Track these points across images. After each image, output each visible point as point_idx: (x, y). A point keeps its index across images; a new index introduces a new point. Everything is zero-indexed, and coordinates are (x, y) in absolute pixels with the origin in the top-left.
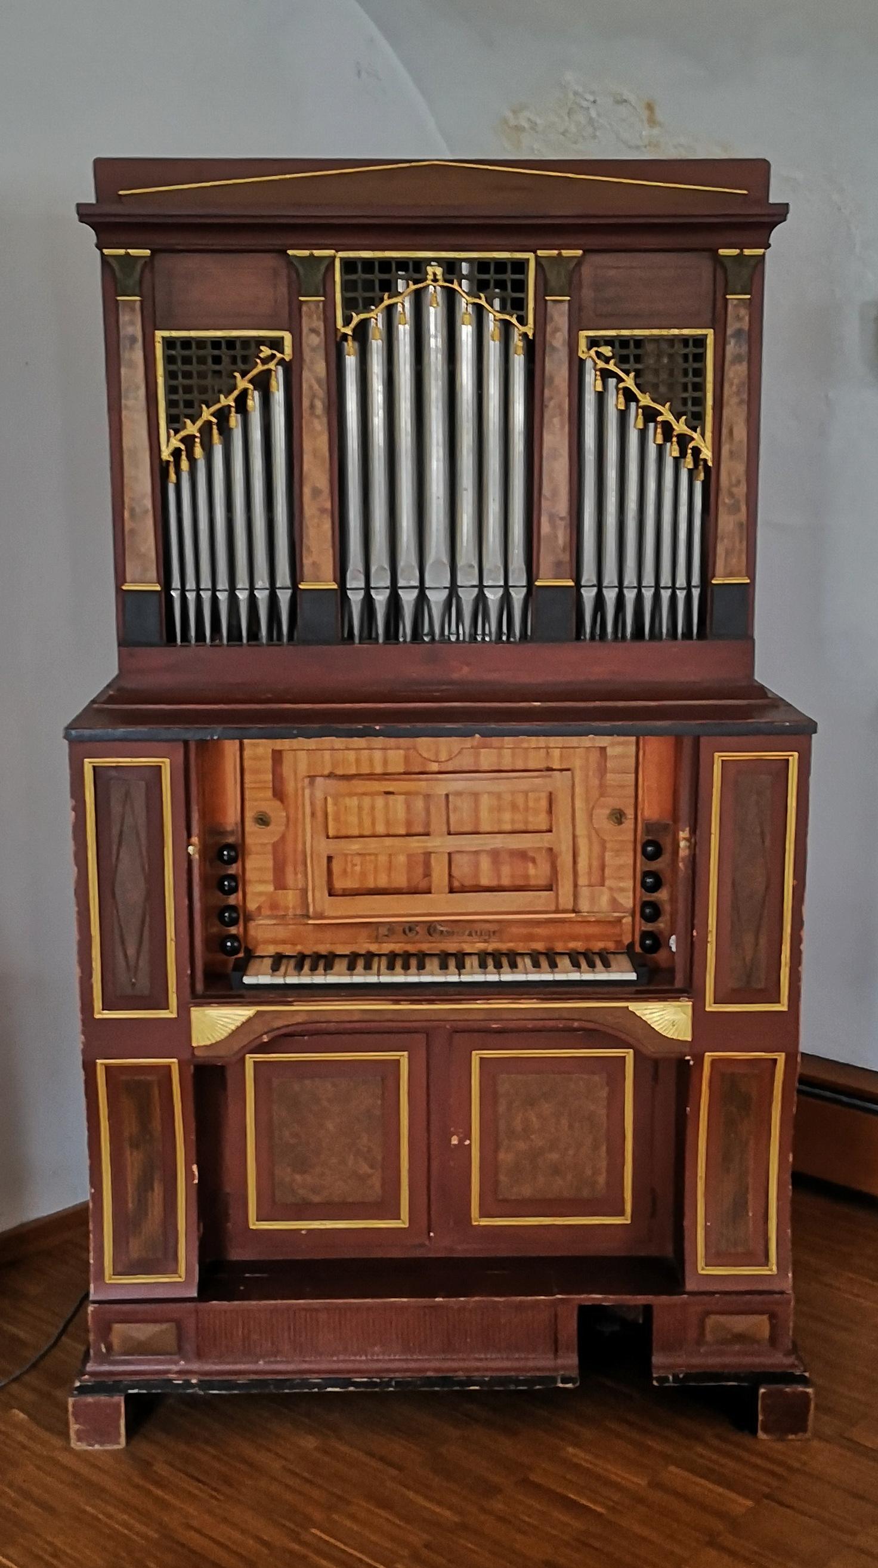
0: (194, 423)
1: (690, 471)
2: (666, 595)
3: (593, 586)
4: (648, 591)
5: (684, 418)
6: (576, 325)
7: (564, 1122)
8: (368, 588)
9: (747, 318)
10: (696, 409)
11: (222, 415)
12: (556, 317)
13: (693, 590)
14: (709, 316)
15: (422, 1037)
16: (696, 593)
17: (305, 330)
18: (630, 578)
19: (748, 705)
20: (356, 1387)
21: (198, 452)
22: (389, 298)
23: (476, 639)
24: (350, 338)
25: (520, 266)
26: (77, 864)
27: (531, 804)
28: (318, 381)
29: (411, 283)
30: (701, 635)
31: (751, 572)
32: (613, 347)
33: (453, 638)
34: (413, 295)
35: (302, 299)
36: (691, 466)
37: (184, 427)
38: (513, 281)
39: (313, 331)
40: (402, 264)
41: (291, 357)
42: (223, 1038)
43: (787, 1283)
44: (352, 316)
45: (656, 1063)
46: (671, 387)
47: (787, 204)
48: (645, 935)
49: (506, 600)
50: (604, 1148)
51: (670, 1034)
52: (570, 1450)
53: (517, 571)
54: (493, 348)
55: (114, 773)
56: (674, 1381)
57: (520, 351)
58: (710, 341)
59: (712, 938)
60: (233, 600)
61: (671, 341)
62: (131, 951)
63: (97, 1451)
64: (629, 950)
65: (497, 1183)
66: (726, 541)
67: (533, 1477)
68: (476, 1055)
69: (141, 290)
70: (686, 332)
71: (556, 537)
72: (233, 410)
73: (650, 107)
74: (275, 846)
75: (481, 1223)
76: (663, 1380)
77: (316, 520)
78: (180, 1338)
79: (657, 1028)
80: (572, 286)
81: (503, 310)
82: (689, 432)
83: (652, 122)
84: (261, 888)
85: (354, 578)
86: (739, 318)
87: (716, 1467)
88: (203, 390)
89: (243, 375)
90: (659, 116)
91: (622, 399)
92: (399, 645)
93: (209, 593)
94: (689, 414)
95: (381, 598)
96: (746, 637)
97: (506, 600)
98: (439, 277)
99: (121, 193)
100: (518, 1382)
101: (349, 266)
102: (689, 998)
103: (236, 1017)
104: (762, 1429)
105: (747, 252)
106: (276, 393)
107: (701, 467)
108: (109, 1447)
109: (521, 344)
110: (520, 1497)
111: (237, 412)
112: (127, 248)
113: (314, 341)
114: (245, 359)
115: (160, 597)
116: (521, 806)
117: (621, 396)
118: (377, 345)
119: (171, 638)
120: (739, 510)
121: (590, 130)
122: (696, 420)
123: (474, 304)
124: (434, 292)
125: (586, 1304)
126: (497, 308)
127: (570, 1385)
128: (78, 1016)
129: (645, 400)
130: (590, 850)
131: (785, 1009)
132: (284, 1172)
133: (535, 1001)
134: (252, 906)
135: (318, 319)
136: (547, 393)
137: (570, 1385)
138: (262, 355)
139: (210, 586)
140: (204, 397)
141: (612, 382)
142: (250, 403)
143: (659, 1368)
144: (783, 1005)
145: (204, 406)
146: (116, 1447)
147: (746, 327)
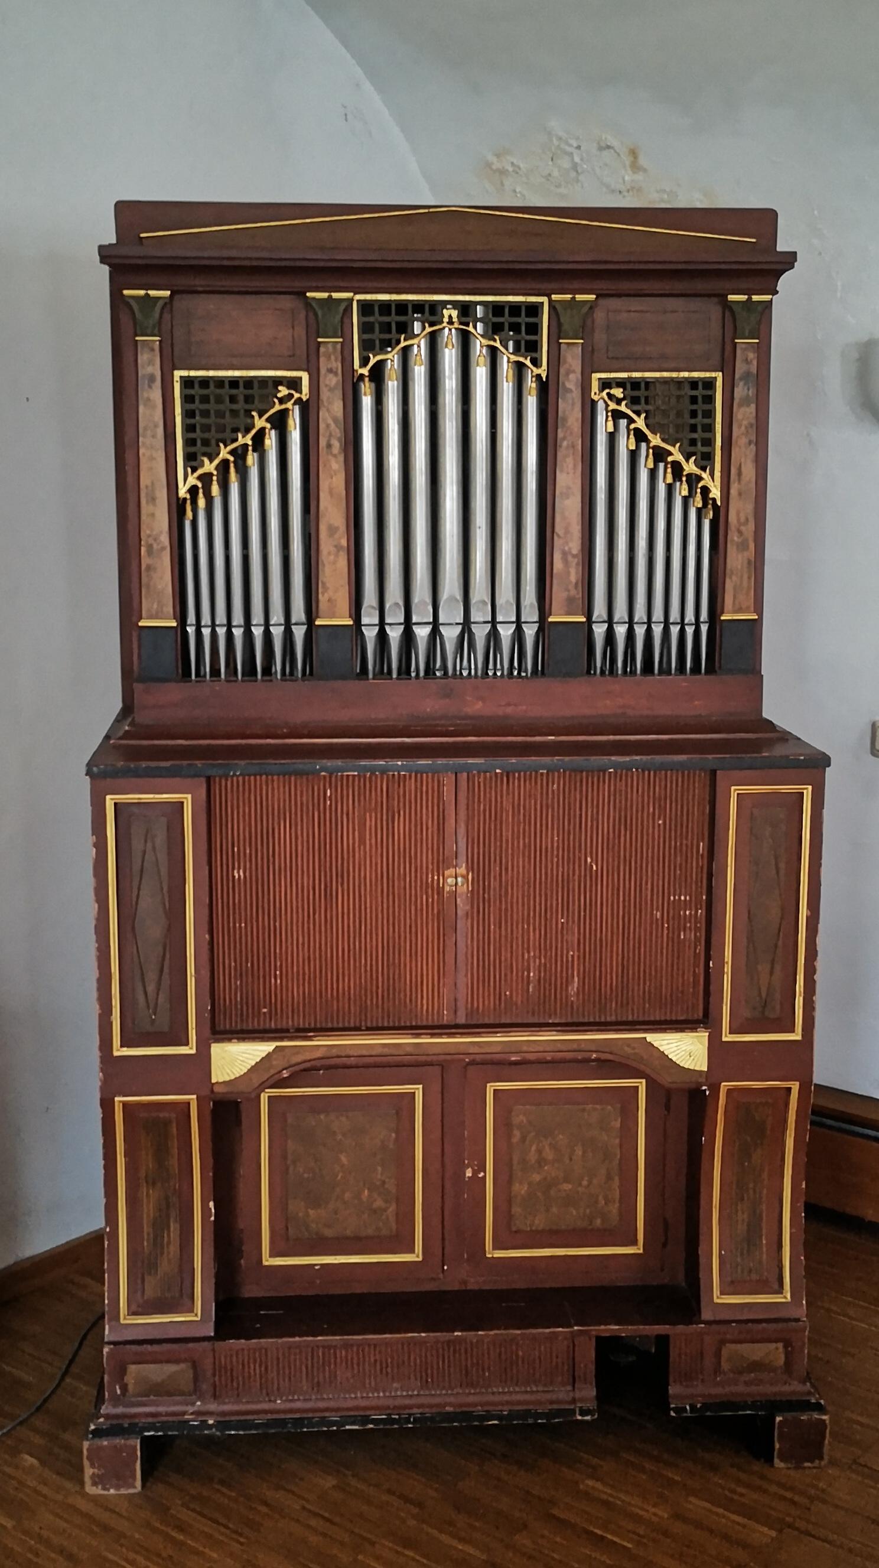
0: (211, 461)
1: (699, 511)
2: (675, 630)
3: (604, 622)
4: (600, 627)
5: (694, 458)
6: (589, 367)
7: (579, 1152)
8: (382, 623)
9: (755, 362)
10: (706, 449)
12: (569, 359)
13: (702, 626)
15: (437, 1070)
16: (704, 628)
17: (323, 371)
18: (640, 613)
19: (757, 739)
20: (384, 1425)
21: (215, 489)
22: (405, 340)
23: (487, 674)
24: (367, 379)
25: (534, 310)
26: (97, 901)
28: (335, 420)
29: (427, 325)
30: (711, 670)
31: (759, 608)
32: (625, 389)
33: (465, 673)
34: (428, 336)
35: (320, 340)
36: (700, 505)
37: (202, 465)
39: (330, 371)
40: (419, 307)
41: (308, 397)
42: (242, 1073)
43: (801, 1312)
45: (669, 1093)
46: (678, 428)
47: (795, 253)
49: (519, 635)
51: (687, 1064)
52: (590, 1482)
53: (528, 608)
54: (507, 389)
55: (135, 810)
57: (534, 392)
58: (719, 384)
59: (728, 969)
60: (248, 635)
61: (679, 383)
62: (151, 988)
63: (112, 1495)
65: (510, 1216)
66: (734, 578)
67: (555, 1512)
68: (491, 1088)
69: (160, 330)
70: (696, 375)
71: (568, 573)
72: (250, 448)
73: (633, 153)
75: (495, 1256)
76: (680, 1410)
77: (332, 557)
79: (674, 1059)
80: (584, 330)
81: (517, 351)
82: (698, 471)
83: (635, 167)
85: (369, 615)
86: (747, 361)
87: (736, 1497)
88: (222, 429)
89: (260, 416)
90: (642, 161)
92: (487, 680)
93: (225, 629)
94: (699, 455)
95: (394, 634)
96: (754, 672)
97: (519, 635)
98: (455, 319)
99: (142, 235)
100: (538, 1415)
104: (779, 1457)
105: (755, 298)
106: (294, 433)
107: (710, 506)
108: (123, 1491)
109: (534, 385)
110: (546, 1533)
111: (254, 451)
112: (147, 290)
113: (331, 381)
117: (632, 436)
118: (392, 386)
119: (187, 673)
120: (747, 548)
121: (573, 174)
122: (705, 461)
123: (489, 346)
124: (449, 336)
125: (603, 1335)
126: (511, 350)
127: (588, 1418)
128: (95, 1055)
129: (656, 440)
131: (799, 1038)
132: (297, 1207)
133: (554, 1033)
135: (336, 360)
136: (560, 434)
137: (588, 1418)
138: (279, 395)
139: (225, 622)
140: (220, 436)
141: (623, 422)
142: (267, 442)
144: (797, 1034)
145: (222, 445)
146: (132, 1491)
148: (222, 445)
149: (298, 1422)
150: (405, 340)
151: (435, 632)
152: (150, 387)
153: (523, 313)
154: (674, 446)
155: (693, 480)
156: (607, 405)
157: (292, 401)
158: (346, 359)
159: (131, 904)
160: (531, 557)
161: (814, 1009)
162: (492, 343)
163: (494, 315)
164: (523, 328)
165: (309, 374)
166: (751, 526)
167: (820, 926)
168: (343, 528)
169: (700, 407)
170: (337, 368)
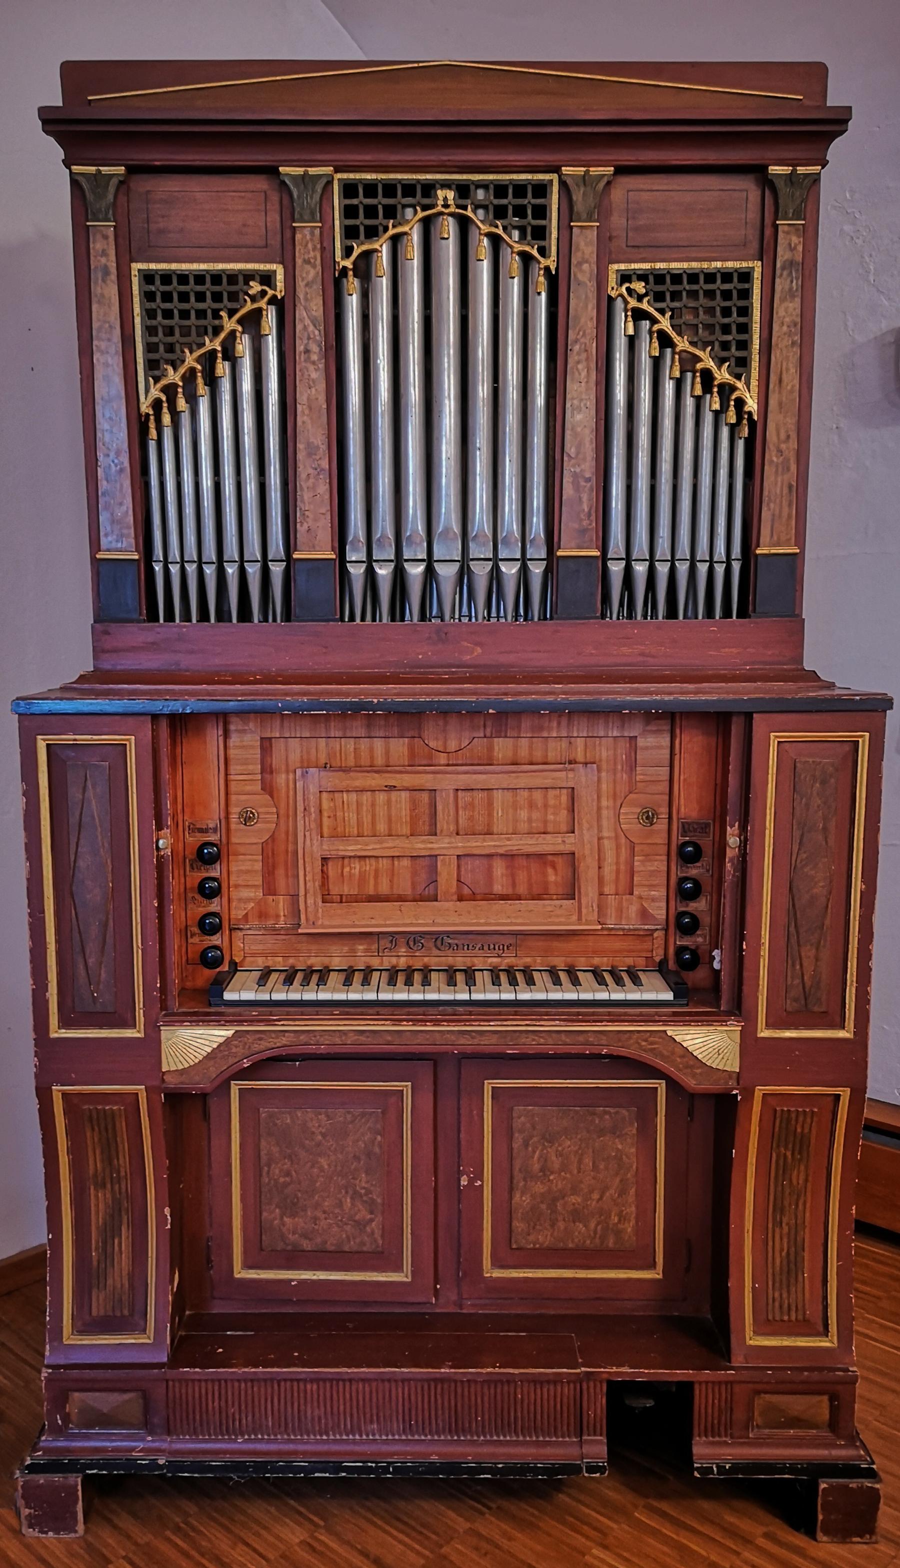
2: (703, 568)
5: (727, 364)
6: (604, 258)
7: (588, 1161)
9: (800, 248)
10: (740, 354)
11: (209, 359)
14: (755, 245)
16: (736, 566)
17: (299, 261)
21: (182, 404)
22: (394, 226)
24: (351, 273)
27: (551, 802)
29: (418, 208)
31: (800, 539)
32: (647, 283)
36: (733, 420)
37: (164, 375)
38: (534, 207)
39: (307, 262)
40: (409, 189)
41: (283, 294)
44: (353, 247)
45: (693, 1096)
47: (851, 107)
48: (680, 950)
50: (632, 1191)
51: (714, 1063)
56: (718, 1474)
59: (765, 952)
62: (91, 961)
64: (662, 968)
68: (488, 1085)
70: (730, 264)
74: (264, 845)
75: (494, 1275)
78: (147, 1410)
84: (245, 893)
85: (355, 550)
89: (230, 316)
91: (656, 344)
93: (195, 566)
94: (733, 360)
98: (451, 202)
99: (90, 98)
101: (349, 189)
102: (738, 1022)
103: (215, 1039)
104: (822, 1531)
107: (745, 422)
111: (224, 359)
114: (233, 297)
115: (139, 567)
116: (540, 804)
117: (655, 340)
129: (682, 344)
130: (618, 855)
132: (272, 1214)
134: (237, 913)
142: (239, 348)
143: (702, 1457)
145: (187, 351)
147: (799, 258)
148: (187, 351)
149: (261, 1467)
150: (394, 226)
151: (430, 573)
152: (104, 281)
153: (530, 194)
154: (704, 351)
155: (726, 390)
156: (626, 302)
157: (266, 299)
158: (326, 251)
159: (70, 865)
160: (539, 483)
161: (868, 1002)
162: (494, 230)
163: (495, 197)
164: (529, 212)
165: (284, 267)
166: (793, 444)
167: (876, 902)
168: (324, 448)
169: (735, 302)
170: (315, 258)
